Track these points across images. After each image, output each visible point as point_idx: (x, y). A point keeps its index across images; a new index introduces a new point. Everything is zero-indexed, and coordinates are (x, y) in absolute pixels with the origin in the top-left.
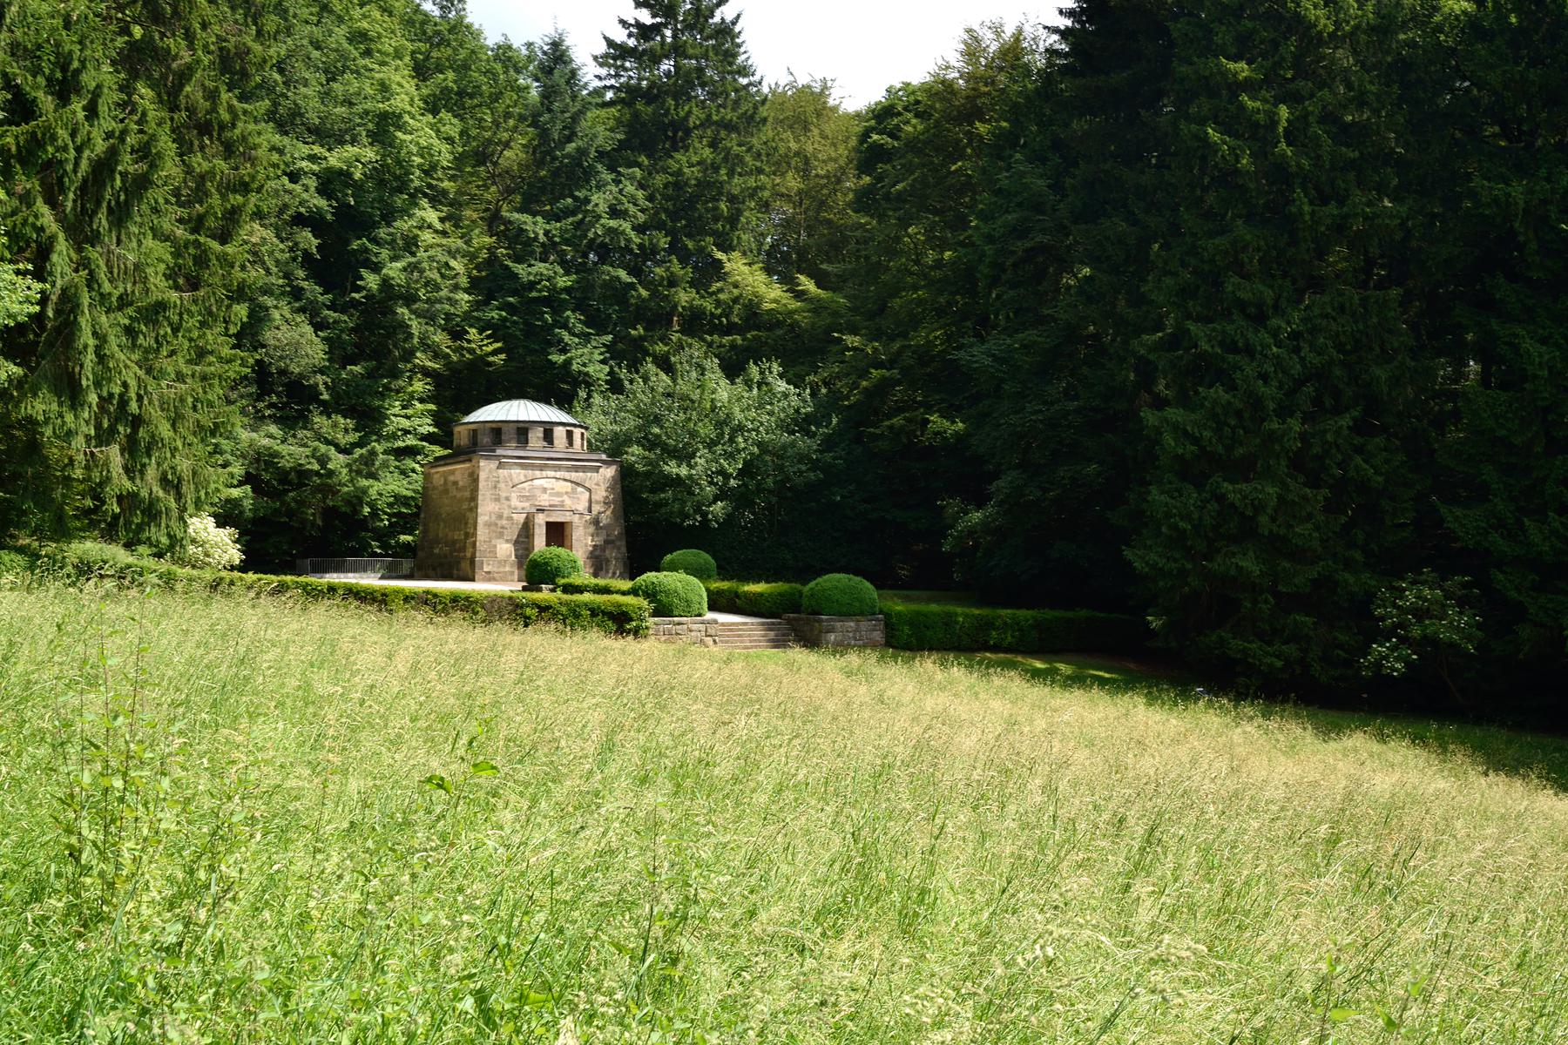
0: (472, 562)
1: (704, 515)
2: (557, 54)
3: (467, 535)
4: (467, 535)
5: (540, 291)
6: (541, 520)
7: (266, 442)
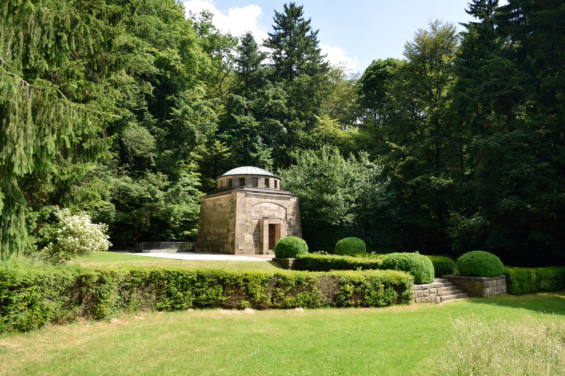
0: (233, 244)
1: (341, 220)
2: (248, 40)
3: (229, 231)
4: (229, 231)
5: (246, 127)
6: (266, 223)
7: (124, 184)
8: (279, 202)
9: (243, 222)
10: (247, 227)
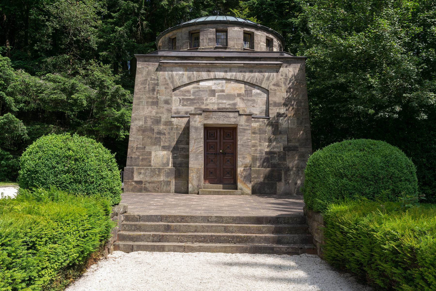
6: (198, 122)
8: (247, 76)
9: (149, 123)
10: (159, 133)
